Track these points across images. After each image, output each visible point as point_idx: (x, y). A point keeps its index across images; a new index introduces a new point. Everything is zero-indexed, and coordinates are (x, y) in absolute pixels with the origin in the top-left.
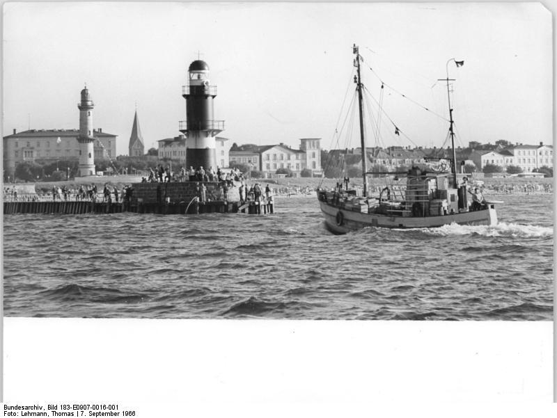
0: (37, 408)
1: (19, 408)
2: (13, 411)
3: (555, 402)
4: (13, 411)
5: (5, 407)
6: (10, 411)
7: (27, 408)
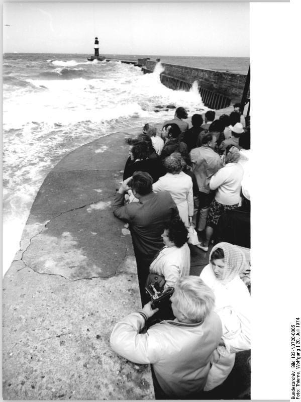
0: (294, 375)
1: (294, 388)
2: (296, 392)
3: (289, 1)
4: (296, 392)
5: (293, 398)
6: (296, 395)
7: (294, 382)
